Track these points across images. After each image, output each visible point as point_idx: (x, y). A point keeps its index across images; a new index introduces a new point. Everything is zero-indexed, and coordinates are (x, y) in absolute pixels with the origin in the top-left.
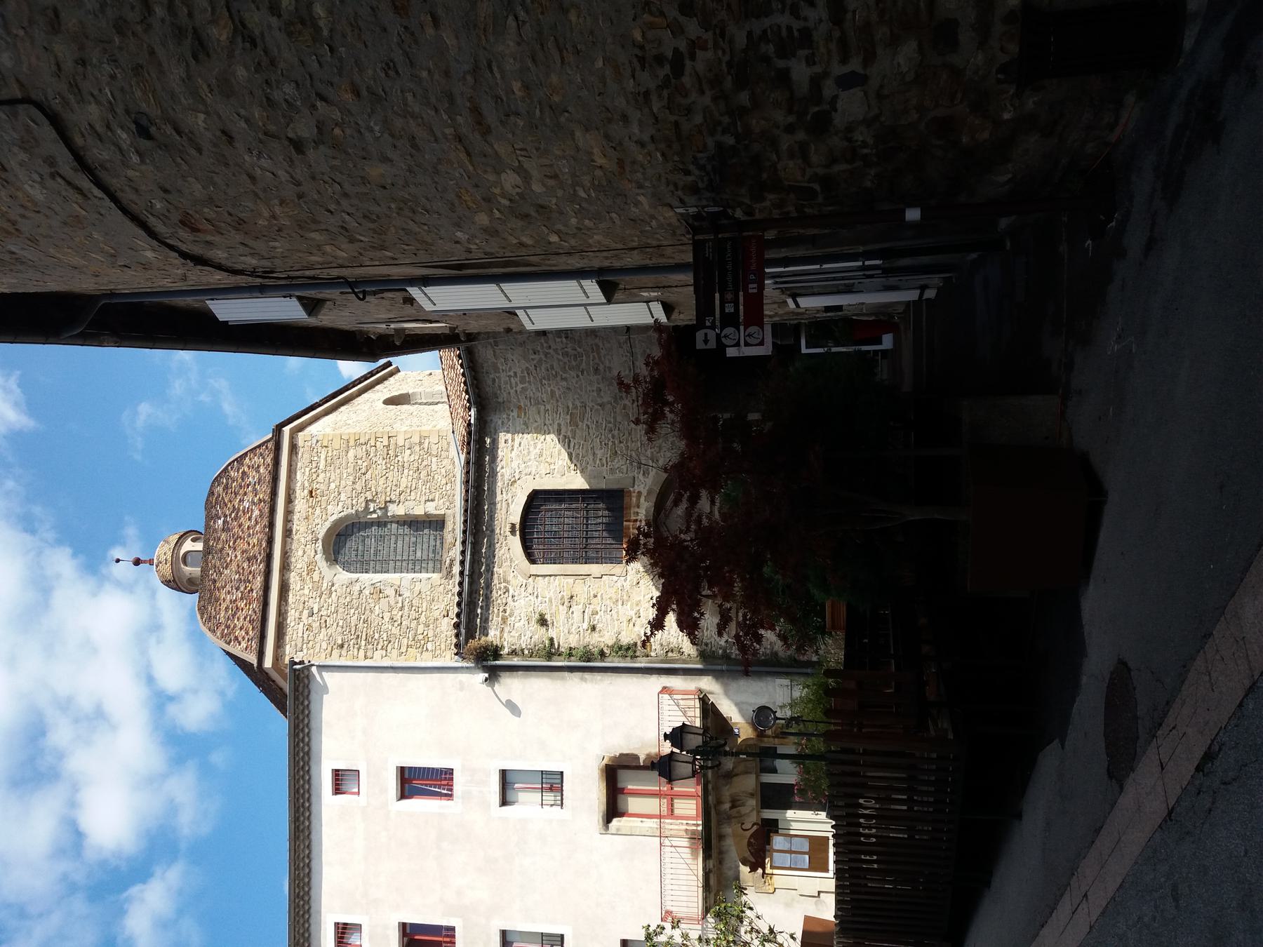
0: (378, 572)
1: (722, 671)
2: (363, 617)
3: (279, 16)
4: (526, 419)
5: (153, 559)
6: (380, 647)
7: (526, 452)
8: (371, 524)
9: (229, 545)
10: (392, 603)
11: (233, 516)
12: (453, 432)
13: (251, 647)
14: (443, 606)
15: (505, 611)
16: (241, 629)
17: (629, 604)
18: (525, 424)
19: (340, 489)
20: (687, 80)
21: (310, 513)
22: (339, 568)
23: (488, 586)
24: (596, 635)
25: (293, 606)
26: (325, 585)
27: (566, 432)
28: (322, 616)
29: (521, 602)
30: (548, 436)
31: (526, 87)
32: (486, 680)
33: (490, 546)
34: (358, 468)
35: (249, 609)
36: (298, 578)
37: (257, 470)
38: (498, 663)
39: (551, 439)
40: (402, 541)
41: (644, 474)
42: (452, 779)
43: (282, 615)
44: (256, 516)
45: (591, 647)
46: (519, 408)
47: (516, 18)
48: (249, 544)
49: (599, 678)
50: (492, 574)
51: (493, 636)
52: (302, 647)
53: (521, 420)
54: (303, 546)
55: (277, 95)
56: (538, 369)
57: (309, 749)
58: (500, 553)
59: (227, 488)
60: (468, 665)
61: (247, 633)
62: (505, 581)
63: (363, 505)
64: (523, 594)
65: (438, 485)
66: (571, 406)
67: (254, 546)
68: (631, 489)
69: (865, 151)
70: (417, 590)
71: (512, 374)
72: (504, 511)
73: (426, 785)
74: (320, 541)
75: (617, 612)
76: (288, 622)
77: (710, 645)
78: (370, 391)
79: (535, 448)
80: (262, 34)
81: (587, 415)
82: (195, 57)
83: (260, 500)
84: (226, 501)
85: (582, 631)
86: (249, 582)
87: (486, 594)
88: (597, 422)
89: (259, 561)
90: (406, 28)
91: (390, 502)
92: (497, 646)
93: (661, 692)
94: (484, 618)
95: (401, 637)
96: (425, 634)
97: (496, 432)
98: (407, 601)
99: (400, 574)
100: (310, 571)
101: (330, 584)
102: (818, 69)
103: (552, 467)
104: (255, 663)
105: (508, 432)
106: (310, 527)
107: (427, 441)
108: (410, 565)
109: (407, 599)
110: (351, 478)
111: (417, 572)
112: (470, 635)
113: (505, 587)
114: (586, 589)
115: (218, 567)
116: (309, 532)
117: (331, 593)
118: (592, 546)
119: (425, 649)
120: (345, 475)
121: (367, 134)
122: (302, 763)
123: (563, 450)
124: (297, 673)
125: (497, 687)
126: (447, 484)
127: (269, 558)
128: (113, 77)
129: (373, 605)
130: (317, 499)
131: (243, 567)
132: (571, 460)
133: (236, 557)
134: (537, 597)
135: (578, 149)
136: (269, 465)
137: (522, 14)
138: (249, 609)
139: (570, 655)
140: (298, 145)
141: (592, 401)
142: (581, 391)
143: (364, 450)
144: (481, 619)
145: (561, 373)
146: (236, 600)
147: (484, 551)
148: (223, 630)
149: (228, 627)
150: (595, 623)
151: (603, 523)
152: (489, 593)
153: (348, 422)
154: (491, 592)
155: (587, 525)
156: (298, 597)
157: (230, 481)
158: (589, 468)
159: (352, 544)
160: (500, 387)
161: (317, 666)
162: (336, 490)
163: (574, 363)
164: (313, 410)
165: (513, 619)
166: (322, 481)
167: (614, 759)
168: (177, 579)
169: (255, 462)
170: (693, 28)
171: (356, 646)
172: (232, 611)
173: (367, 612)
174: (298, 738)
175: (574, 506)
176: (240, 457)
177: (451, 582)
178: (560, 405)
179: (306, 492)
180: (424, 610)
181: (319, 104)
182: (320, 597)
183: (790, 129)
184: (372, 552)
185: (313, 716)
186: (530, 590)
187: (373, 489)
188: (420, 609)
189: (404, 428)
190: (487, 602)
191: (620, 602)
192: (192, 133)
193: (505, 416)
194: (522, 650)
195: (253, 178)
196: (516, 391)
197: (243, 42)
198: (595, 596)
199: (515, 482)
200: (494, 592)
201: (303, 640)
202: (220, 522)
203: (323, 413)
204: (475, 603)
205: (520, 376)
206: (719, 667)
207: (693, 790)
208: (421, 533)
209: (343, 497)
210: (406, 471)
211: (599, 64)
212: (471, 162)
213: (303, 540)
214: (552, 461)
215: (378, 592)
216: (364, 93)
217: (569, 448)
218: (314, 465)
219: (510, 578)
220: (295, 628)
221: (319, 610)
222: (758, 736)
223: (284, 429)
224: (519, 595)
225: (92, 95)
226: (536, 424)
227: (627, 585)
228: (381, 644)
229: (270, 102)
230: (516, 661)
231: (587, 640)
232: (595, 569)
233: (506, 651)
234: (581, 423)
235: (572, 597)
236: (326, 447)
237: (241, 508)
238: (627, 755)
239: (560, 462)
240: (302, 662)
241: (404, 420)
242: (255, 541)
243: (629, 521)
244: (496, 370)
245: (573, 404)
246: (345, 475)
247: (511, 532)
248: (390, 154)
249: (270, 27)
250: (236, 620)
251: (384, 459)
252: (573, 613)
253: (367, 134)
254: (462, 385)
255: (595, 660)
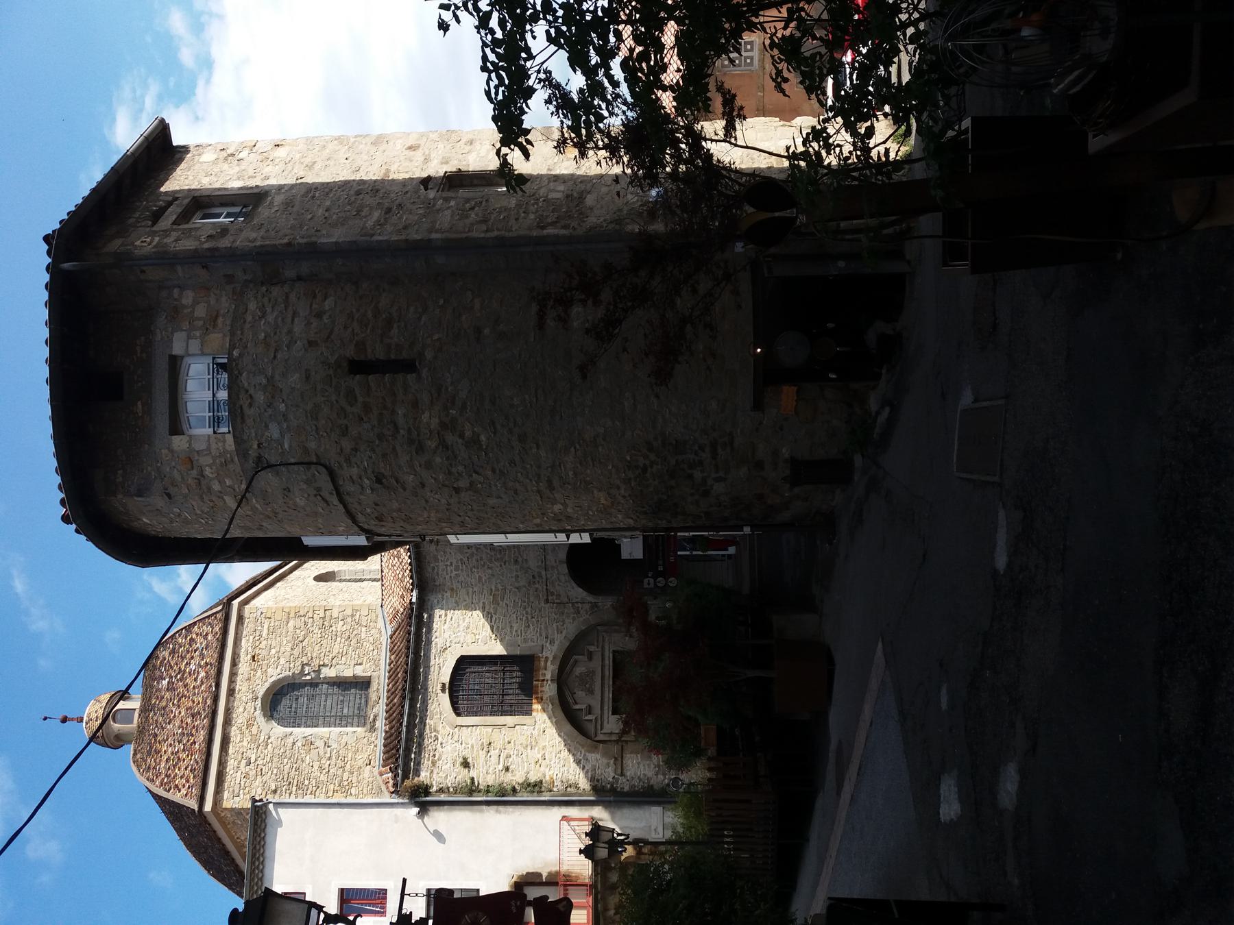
0: (309, 727)
1: (610, 802)
2: (295, 766)
3: (463, 439)
4: (457, 599)
5: (83, 718)
6: (309, 792)
7: (456, 625)
8: (305, 684)
9: (173, 703)
10: (322, 753)
11: (178, 677)
12: (382, 606)
13: (192, 793)
14: (366, 756)
15: (434, 756)
16: (182, 777)
17: (537, 748)
18: (456, 602)
19: (280, 655)
20: (648, 475)
21: (252, 675)
22: (274, 723)
23: (421, 735)
24: (509, 774)
25: (233, 756)
26: (262, 738)
27: (489, 609)
28: (258, 765)
29: (448, 748)
30: (474, 612)
31: (575, 474)
32: (419, 813)
33: (424, 702)
34: (296, 637)
35: (191, 759)
36: (238, 732)
37: (205, 637)
38: (428, 798)
39: (477, 614)
40: (329, 701)
41: (550, 643)
42: (385, 898)
43: (222, 764)
44: (202, 678)
45: (505, 785)
46: (452, 589)
47: (575, 448)
48: (193, 702)
49: (511, 810)
50: (425, 725)
51: (424, 776)
52: (239, 793)
53: (453, 599)
54: (244, 704)
55: (454, 470)
56: (470, 560)
57: (263, 876)
58: (432, 707)
59: (174, 652)
60: (403, 801)
61: (188, 781)
62: (435, 731)
63: (300, 668)
64: (450, 741)
65: (366, 650)
66: (493, 588)
67: (199, 703)
68: (540, 655)
69: (725, 504)
70: (344, 741)
71: (449, 564)
72: (436, 672)
73: (362, 904)
74: (259, 699)
75: (527, 756)
76: (228, 771)
77: (600, 781)
78: (299, 569)
79: (464, 621)
80: (452, 445)
81: (506, 596)
82: (416, 453)
83: (207, 664)
84: (172, 664)
85: (498, 772)
86: (192, 735)
87: (419, 742)
88: (514, 601)
89: (203, 716)
90: (523, 448)
91: (323, 665)
92: (427, 785)
93: (562, 820)
94: (416, 762)
95: (328, 784)
96: (349, 780)
97: (432, 609)
98: (335, 752)
99: (328, 728)
100: (249, 726)
101: (267, 737)
102: (705, 474)
103: (477, 637)
104: (196, 808)
105: (442, 609)
106: (251, 687)
107: (358, 613)
108: (338, 721)
109: (335, 750)
110: (290, 645)
111: (344, 727)
112: (406, 776)
113: (435, 736)
114: (502, 736)
115: (160, 723)
116: (250, 691)
117: (267, 745)
118: (507, 702)
119: (349, 793)
120: (285, 642)
121: (493, 487)
122: (256, 888)
123: (486, 623)
124: (257, 809)
125: (426, 818)
126: (374, 650)
127: (214, 713)
128: (371, 457)
129: (304, 755)
130: (259, 663)
131: (187, 723)
132: (492, 631)
133: (180, 713)
134: (461, 744)
135: (594, 497)
136: (217, 633)
137: (578, 447)
138: (191, 759)
139: (488, 791)
140: (457, 490)
141: (511, 585)
142: (503, 577)
143: (303, 621)
144: (414, 762)
145: (488, 563)
146: (178, 752)
147: (418, 706)
148: (163, 779)
149: (168, 776)
150: (508, 765)
151: (516, 682)
152: (421, 741)
153: (287, 597)
154: (424, 740)
155: (503, 684)
156: (237, 749)
157: (177, 646)
158: (507, 638)
159: (285, 702)
160: (438, 574)
161: (274, 803)
162: (276, 655)
163: (499, 556)
164: (255, 586)
165: (441, 762)
166: (264, 647)
167: (522, 877)
168: (105, 735)
169: (203, 630)
170: (652, 457)
171: (288, 791)
172: (173, 761)
173: (299, 762)
174: (254, 866)
175: (493, 668)
176: (188, 626)
177: (374, 735)
178: (485, 587)
179: (249, 656)
180: (349, 759)
181: (474, 475)
182: (258, 748)
183: (692, 495)
184: (304, 709)
185: (267, 846)
186: (456, 738)
187: (309, 655)
188: (346, 759)
189: (338, 603)
190: (419, 748)
191: (529, 748)
192: (404, 482)
193: (440, 596)
194: (448, 788)
195: (427, 501)
196: (451, 577)
197: (443, 448)
198: (509, 743)
199: (446, 649)
200: (426, 740)
201: (240, 787)
202: (165, 683)
203: (263, 589)
204: (409, 749)
205: (455, 566)
206: (607, 799)
207: (585, 901)
208: (349, 692)
209: (282, 661)
210: (339, 639)
211: (610, 467)
212: (542, 501)
213: (244, 698)
214: (477, 632)
215: (309, 743)
216: (498, 472)
217: (491, 622)
218: (258, 634)
219: (440, 728)
220: (233, 776)
221: (256, 760)
222: (637, 854)
223: (233, 602)
224: (446, 742)
225: (356, 464)
226: (465, 603)
227: (535, 733)
228: (310, 789)
229: (450, 473)
230: (443, 797)
231: (502, 779)
232: (509, 720)
233: (435, 789)
234: (501, 603)
235: (490, 743)
236: (269, 618)
237: (187, 670)
238: (533, 873)
239: (484, 633)
240: (261, 800)
241: (337, 596)
242: (200, 699)
243: (538, 680)
244: (436, 560)
245: (496, 587)
246: (285, 642)
247: (441, 690)
248: (502, 496)
249: (457, 442)
250: (177, 769)
251: (319, 629)
252: (490, 756)
253: (493, 487)
254: (408, 572)
255: (508, 795)
